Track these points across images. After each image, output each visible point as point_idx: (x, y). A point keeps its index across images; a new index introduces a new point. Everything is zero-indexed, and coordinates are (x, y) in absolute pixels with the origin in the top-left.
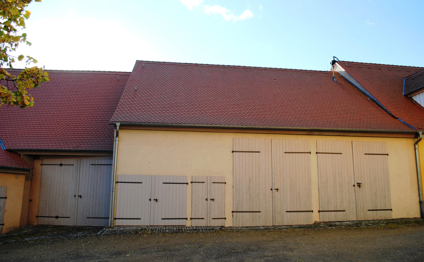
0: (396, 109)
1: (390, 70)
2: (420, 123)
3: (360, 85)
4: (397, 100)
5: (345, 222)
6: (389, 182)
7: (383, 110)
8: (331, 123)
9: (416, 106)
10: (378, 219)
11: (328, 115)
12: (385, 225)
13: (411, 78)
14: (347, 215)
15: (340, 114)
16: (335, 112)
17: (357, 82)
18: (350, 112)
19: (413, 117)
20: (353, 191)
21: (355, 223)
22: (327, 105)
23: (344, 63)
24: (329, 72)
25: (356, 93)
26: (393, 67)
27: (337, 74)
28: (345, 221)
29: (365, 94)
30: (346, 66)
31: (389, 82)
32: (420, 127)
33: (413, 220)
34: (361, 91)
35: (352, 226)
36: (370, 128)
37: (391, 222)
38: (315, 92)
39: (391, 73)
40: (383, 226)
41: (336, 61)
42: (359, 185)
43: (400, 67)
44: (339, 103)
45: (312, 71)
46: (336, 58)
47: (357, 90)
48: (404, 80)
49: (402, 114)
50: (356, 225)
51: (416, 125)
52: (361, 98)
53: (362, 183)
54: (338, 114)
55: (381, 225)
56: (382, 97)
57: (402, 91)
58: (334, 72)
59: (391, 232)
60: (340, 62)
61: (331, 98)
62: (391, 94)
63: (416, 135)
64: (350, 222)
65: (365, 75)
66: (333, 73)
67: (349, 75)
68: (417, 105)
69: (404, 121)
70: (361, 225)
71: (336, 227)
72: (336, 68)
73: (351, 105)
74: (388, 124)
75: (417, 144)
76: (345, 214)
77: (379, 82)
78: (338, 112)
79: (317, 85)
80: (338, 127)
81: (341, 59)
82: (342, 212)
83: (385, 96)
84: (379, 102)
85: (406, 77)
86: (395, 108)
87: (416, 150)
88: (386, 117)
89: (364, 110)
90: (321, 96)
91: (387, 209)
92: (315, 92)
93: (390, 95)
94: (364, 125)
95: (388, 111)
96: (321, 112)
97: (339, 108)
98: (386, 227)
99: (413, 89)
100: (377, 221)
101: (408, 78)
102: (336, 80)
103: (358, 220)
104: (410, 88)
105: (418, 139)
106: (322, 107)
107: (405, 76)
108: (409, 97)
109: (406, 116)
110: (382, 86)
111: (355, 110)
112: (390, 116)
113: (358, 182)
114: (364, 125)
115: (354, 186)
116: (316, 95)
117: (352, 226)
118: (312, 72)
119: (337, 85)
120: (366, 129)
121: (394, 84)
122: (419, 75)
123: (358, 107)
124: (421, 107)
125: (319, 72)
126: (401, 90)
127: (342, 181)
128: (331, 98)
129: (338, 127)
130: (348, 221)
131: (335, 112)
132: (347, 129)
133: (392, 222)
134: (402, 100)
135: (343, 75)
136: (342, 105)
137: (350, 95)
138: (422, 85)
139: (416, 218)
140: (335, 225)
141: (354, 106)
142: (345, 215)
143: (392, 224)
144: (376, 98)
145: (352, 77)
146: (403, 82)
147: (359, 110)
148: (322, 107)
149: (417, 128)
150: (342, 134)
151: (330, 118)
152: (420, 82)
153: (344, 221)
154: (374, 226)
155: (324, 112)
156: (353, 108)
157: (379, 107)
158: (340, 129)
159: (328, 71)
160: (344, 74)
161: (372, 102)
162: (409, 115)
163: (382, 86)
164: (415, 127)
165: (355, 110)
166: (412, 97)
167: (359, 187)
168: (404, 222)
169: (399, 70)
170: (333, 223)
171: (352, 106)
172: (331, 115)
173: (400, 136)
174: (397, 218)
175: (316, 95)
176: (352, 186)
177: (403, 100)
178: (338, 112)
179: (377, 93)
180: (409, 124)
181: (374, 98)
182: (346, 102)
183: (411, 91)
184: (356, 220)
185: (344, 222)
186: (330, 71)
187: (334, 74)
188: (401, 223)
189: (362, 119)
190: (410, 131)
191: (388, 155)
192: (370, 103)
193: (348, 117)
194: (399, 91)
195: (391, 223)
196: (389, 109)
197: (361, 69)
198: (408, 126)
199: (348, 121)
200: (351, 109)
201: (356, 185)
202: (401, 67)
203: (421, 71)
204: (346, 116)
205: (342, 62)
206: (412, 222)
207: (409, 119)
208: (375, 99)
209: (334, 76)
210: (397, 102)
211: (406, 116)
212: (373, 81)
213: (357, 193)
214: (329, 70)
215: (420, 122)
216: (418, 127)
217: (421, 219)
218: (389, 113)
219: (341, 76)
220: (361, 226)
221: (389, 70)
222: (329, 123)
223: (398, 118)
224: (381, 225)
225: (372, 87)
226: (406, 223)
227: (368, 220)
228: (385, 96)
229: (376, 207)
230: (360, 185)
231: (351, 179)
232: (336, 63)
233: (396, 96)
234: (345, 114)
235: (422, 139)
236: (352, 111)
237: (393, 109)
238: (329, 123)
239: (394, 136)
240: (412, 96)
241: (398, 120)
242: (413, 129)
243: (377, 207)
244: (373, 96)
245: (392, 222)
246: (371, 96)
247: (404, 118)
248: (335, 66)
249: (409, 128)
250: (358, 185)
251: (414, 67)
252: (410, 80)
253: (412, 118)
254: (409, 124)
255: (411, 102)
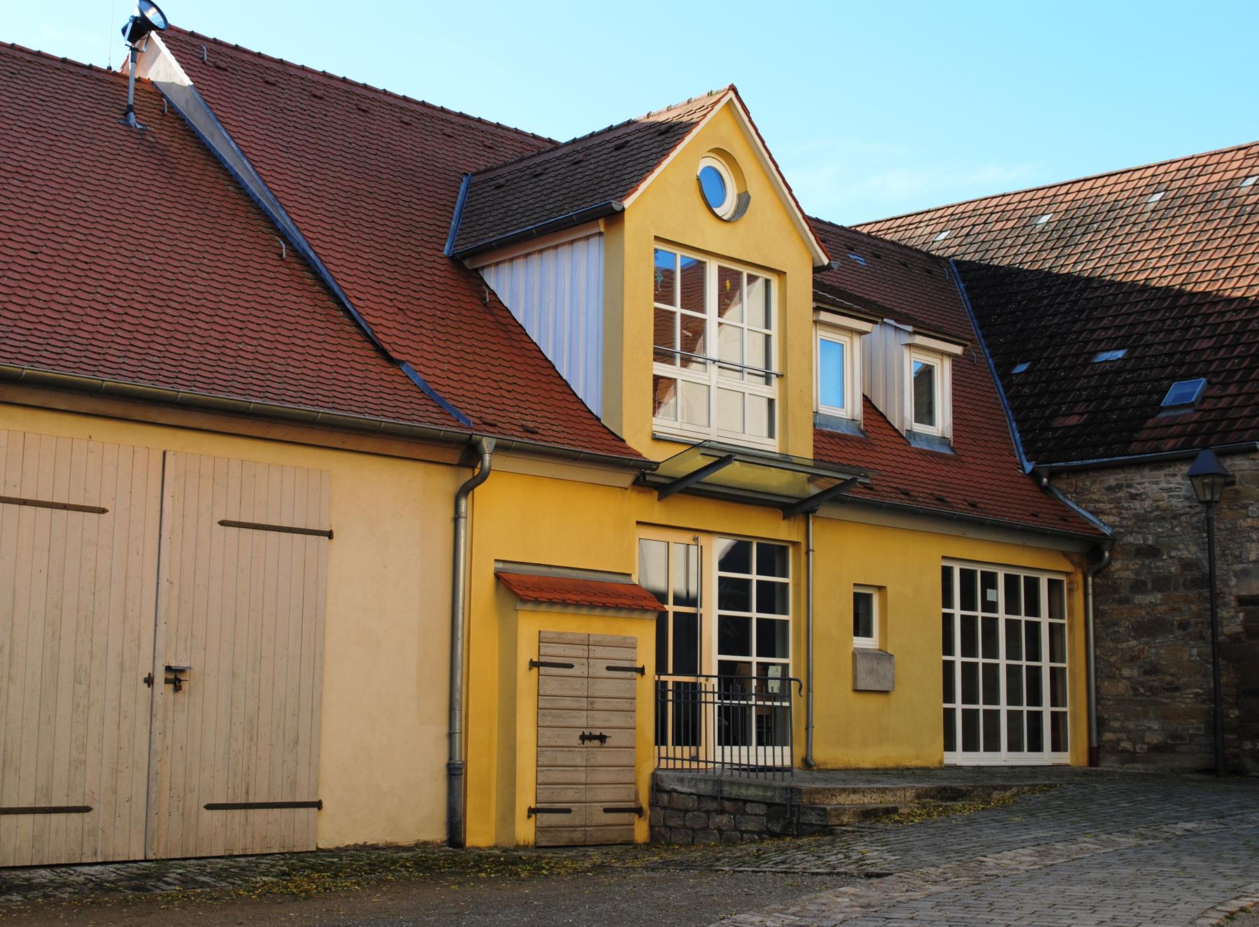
0: (399, 318)
1: (407, 124)
2: (494, 399)
3: (254, 173)
4: (412, 273)
5: (86, 869)
6: (322, 668)
7: (341, 313)
8: (71, 345)
9: (490, 318)
10: (250, 852)
11: (64, 300)
12: (274, 880)
13: (492, 179)
14: (100, 832)
15: (124, 304)
16: (99, 290)
17: (239, 153)
18: (181, 299)
19: (468, 364)
20: (143, 708)
21: (135, 871)
22: (66, 246)
23: (195, 41)
24: (115, 73)
25: (227, 211)
26: (404, 104)
27: (153, 91)
28: (84, 861)
29: (271, 222)
30: (204, 63)
31: (393, 184)
32: (489, 418)
33: (411, 854)
34: (253, 201)
35: (111, 889)
36: (261, 395)
37: (308, 868)
38: (13, 169)
39: (410, 142)
40: (265, 883)
41: (153, 27)
42: (176, 677)
43: (455, 119)
44: (133, 248)
45: (21, 49)
46: (153, 10)
47: (233, 195)
48: (463, 186)
49: (425, 347)
50: (133, 883)
51: (477, 408)
52: (245, 238)
53: (190, 668)
54: (116, 301)
55: (258, 878)
56: (346, 250)
57: (443, 236)
58: (138, 80)
59: (285, 916)
60: (170, 34)
61: (96, 214)
62: (389, 242)
63: (469, 454)
64: (111, 868)
65: (287, 128)
66: (132, 84)
67: (208, 111)
68: (496, 311)
69: (427, 378)
70: (159, 880)
71: (25, 897)
72: (153, 62)
73: (194, 267)
74: (353, 385)
75: (466, 495)
76: (86, 826)
77: (347, 172)
78: (119, 294)
79: (30, 132)
80: (101, 368)
81: (182, 20)
82: (74, 816)
83: (360, 247)
84: (328, 269)
85: (474, 170)
86: (396, 310)
87: (462, 521)
88: (350, 351)
89: (249, 298)
90: (43, 195)
91: (298, 800)
92: (13, 169)
93: (385, 246)
94: (237, 378)
95: (363, 324)
96: (27, 277)
97: (128, 273)
98: (275, 890)
99: (491, 234)
100: (243, 859)
101: (483, 177)
102: (139, 126)
103: (154, 857)
104: (477, 228)
105: (474, 473)
106: (39, 256)
107: (472, 165)
108: (466, 269)
109: (438, 357)
110: (358, 198)
111: (207, 296)
112: (370, 346)
113: (173, 664)
114: (237, 378)
115: (149, 681)
116: (16, 182)
117: (115, 890)
118: (18, 54)
119: (140, 152)
120: (242, 398)
121: (413, 194)
122: (528, 172)
123: (224, 280)
124: (512, 322)
125: (59, 65)
126: (441, 230)
127: (91, 653)
128: (96, 214)
129: (101, 368)
130: (100, 860)
131: (99, 290)
132: (144, 386)
133: (313, 868)
134: (437, 279)
135: (180, 103)
136: (147, 258)
137: (197, 217)
138: (530, 223)
139: (425, 843)
140: (30, 886)
141: (205, 275)
142: (86, 831)
143: (307, 876)
144: (317, 250)
145: (219, 125)
146: (454, 194)
147: (223, 299)
148: (39, 256)
149: (478, 421)
150: (117, 409)
151: (68, 316)
152: (523, 204)
153: (78, 861)
154: (224, 884)
155: (45, 280)
156: (201, 282)
157: (325, 297)
158: (109, 382)
159: (110, 68)
160: (187, 102)
161: (296, 266)
162: (453, 353)
163: (358, 198)
164: (469, 412)
165: (207, 296)
166: (481, 273)
167: (172, 686)
168: (369, 864)
169: (448, 131)
170: (18, 873)
171: (192, 274)
172: (76, 302)
173: (397, 449)
174: (341, 846)
175: (16, 182)
176: (141, 681)
177: (442, 280)
178: (119, 294)
179: (328, 227)
180: (447, 396)
181: (310, 246)
182: (168, 248)
183: (480, 243)
184: (143, 858)
185: (79, 869)
186: (119, 70)
187: (131, 91)
188: (354, 870)
189: (233, 346)
190: (446, 428)
191: (330, 535)
192: (287, 271)
193: (164, 325)
194: (430, 234)
195: (304, 868)
196: (369, 311)
197: (272, 92)
198: (440, 404)
199: (161, 348)
200: (187, 286)
201: (160, 677)
202: (461, 121)
203: (539, 154)
204: (155, 316)
205: (188, 38)
206: (401, 866)
207: (451, 375)
208: (312, 254)
209: (131, 102)
210: (410, 285)
211: (438, 357)
212: (319, 164)
213: (160, 715)
214: (117, 68)
215: (496, 393)
216: (484, 415)
217: (448, 848)
218: (367, 335)
219: (171, 106)
220: (159, 888)
221: (402, 122)
222: (60, 344)
223: (402, 362)
224: (257, 882)
225: (312, 191)
226: (373, 867)
227: (203, 855)
228: (360, 247)
229: (247, 793)
230: (179, 676)
231: (139, 647)
232: (153, 34)
233: (413, 255)
234: (151, 307)
235: (491, 472)
236: (188, 299)
237: (385, 316)
238: (60, 344)
239: (369, 444)
240: (483, 268)
241: (401, 374)
242: (458, 421)
243: (251, 791)
244: (304, 236)
245: (313, 868)
246: (297, 234)
247: (429, 364)
248: (144, 49)
249: (442, 416)
250: (171, 676)
251: (516, 131)
252: (488, 189)
253: (467, 371)
254: (447, 396)
255: (472, 296)
